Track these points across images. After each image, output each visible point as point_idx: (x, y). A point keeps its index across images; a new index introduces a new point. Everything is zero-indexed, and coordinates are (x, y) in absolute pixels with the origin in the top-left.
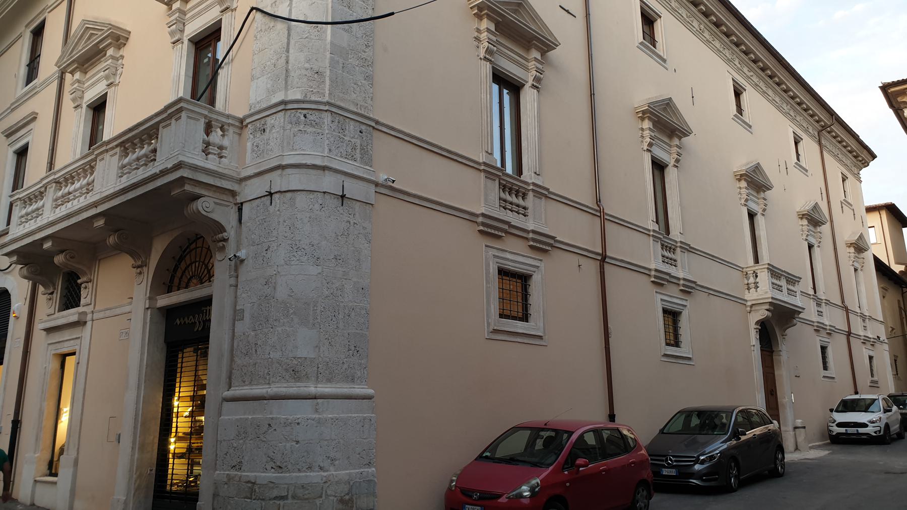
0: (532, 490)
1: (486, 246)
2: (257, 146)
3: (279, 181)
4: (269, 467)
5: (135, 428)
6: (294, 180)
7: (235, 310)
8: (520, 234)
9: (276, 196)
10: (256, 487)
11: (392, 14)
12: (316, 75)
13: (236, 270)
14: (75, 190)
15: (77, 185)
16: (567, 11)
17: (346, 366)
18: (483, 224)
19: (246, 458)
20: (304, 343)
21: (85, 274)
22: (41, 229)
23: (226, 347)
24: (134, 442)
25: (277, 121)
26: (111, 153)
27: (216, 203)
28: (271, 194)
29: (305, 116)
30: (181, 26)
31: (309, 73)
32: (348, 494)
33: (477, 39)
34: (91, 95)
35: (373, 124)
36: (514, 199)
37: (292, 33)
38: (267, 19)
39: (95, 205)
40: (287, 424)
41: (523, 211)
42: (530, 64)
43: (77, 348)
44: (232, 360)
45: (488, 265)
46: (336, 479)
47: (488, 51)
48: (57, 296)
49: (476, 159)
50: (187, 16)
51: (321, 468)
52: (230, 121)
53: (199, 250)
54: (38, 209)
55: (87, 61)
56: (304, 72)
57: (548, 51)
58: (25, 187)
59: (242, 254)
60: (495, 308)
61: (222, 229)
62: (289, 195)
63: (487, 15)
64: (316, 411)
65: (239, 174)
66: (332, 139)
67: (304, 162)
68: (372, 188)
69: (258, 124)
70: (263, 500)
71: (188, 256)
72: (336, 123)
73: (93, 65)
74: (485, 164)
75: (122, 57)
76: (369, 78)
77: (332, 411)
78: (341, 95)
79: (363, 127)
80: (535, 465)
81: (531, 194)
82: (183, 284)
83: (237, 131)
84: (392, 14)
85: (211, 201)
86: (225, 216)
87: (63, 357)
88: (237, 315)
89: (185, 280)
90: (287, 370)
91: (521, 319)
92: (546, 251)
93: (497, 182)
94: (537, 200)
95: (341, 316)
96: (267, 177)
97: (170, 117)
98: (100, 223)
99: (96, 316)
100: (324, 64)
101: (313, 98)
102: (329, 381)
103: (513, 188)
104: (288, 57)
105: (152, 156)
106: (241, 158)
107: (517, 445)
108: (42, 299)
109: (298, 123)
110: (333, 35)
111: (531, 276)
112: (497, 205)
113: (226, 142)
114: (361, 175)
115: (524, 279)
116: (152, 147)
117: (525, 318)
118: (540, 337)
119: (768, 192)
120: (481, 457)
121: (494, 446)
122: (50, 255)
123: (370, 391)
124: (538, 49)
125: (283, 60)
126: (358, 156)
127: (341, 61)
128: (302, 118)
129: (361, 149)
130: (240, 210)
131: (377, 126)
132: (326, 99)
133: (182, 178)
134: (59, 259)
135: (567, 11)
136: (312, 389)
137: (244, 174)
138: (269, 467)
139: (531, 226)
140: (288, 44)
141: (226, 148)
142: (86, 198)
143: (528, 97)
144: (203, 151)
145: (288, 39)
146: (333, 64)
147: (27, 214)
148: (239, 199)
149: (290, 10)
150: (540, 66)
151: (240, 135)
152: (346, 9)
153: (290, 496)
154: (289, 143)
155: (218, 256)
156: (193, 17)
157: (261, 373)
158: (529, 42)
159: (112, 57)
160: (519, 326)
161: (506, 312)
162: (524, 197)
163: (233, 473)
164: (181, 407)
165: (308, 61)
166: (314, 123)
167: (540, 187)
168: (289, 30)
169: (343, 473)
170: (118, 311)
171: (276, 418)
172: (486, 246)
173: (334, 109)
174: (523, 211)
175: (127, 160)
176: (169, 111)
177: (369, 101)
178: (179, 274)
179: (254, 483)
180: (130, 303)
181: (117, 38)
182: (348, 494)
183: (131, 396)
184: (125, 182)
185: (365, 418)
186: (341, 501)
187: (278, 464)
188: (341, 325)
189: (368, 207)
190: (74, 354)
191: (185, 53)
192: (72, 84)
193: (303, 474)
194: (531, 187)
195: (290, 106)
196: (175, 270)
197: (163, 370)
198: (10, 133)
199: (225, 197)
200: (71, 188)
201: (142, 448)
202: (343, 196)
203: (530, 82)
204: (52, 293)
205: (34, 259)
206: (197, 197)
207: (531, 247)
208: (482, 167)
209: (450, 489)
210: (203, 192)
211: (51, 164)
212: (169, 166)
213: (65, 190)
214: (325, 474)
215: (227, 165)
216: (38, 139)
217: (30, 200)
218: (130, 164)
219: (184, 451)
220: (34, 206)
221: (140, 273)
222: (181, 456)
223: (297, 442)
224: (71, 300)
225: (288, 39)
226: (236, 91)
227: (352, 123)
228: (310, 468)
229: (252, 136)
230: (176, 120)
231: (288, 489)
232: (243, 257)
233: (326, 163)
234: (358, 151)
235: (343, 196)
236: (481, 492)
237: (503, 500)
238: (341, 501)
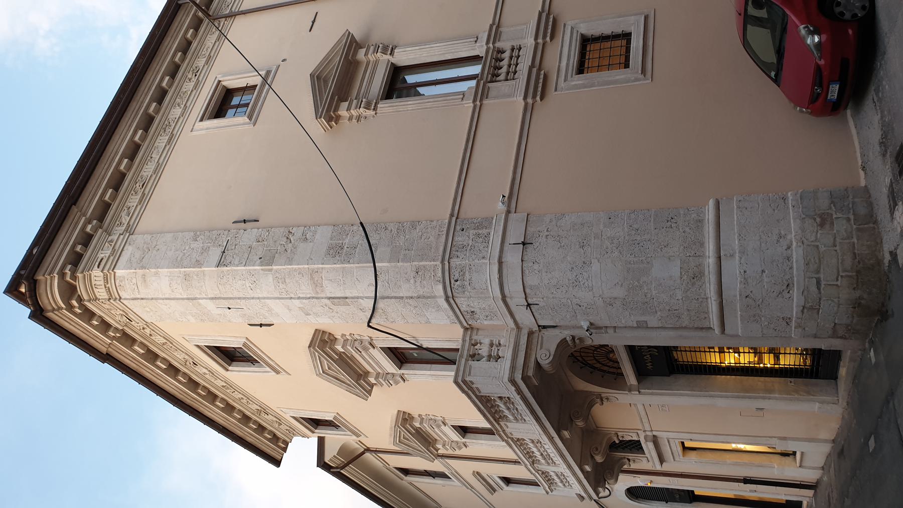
0: (812, 33)
1: (556, 90)
3: (517, 300)
4: (788, 295)
5: (750, 398)
6: (514, 287)
7: (638, 327)
8: (540, 51)
9: (530, 301)
10: (807, 305)
11: (361, 223)
13: (600, 328)
14: (539, 451)
15: (534, 450)
16: (313, 22)
17: (687, 229)
18: (534, 97)
19: (779, 314)
20: (667, 271)
21: (610, 438)
22: (574, 474)
23: (672, 333)
24: (764, 398)
25: (463, 303)
26: (505, 428)
27: (541, 348)
28: (529, 305)
29: (457, 281)
30: (389, 376)
31: (419, 280)
32: (815, 219)
33: (359, 118)
34: (455, 436)
35: (454, 219)
36: (505, 63)
37: (386, 295)
38: (376, 315)
39: (551, 439)
40: (745, 282)
41: (516, 50)
42: (371, 59)
43: (677, 441)
44: (685, 328)
45: (576, 87)
46: (800, 232)
47: (367, 107)
48: (631, 456)
49: (471, 110)
50: (379, 371)
51: (789, 247)
52: (468, 339)
53: (583, 354)
54: (557, 475)
55: (426, 441)
56: (418, 284)
57: (356, 41)
59: (585, 325)
60: (619, 74)
61: (564, 341)
62: (528, 291)
63: (334, 112)
64: (732, 256)
65: (512, 329)
67: (497, 280)
68: (512, 216)
69: (467, 317)
70: (820, 299)
71: (586, 359)
72: (459, 254)
73: (429, 435)
74: (474, 101)
75: (420, 416)
76: (414, 225)
77: (731, 241)
78: (433, 250)
79: (458, 228)
80: (784, 30)
81: (498, 45)
82: (616, 365)
83: (475, 332)
84: (361, 223)
85: (539, 352)
86: (551, 340)
87: (685, 448)
88: (642, 326)
89: (611, 364)
90: (693, 284)
91: (629, 42)
92: (555, 21)
93: (490, 85)
94: (504, 37)
95: (639, 238)
96: (513, 308)
97: (471, 389)
98: (566, 434)
99: (647, 428)
100: (408, 267)
101: (440, 274)
102: (702, 245)
103: (495, 66)
104: (407, 298)
105: (508, 401)
106: (498, 328)
107: (761, 37)
108: (634, 466)
109: (463, 286)
110: (382, 261)
111: (582, 35)
112: (513, 82)
113: (486, 341)
114: (502, 224)
115: (586, 41)
116: (498, 400)
117: (627, 36)
118: (646, 18)
120: (776, 81)
122: (596, 466)
123: (711, 203)
124: (355, 53)
125: (411, 301)
126: (485, 231)
127: (403, 252)
128: (458, 283)
130: (544, 327)
131: (455, 215)
132: (439, 263)
133: (523, 379)
134: (599, 459)
135: (313, 22)
136: (711, 261)
137: (512, 325)
138: (788, 295)
139: (530, 42)
140: (396, 298)
141: (492, 341)
143: (402, 58)
145: (392, 298)
146: (410, 260)
147: (562, 482)
148: (536, 328)
149: (366, 298)
150: (372, 48)
151: (478, 329)
152: (357, 250)
154: (482, 293)
155: (588, 342)
156: (380, 367)
158: (351, 63)
159: (421, 423)
160: (636, 43)
161: (623, 60)
162: (501, 51)
163: (793, 324)
164: (730, 359)
165: (408, 280)
167: (489, 36)
168: (383, 298)
169: (794, 225)
170: (643, 413)
171: (740, 291)
172: (556, 90)
173: (446, 258)
174: (516, 50)
175: (511, 417)
176: (466, 389)
177: (434, 223)
178: (606, 368)
179: (804, 307)
180: (635, 405)
181: (405, 420)
182: (815, 219)
183: (721, 402)
184: (529, 418)
185: (738, 207)
186: (822, 225)
187: (785, 287)
188: (647, 237)
189: (530, 219)
190: (683, 443)
191: (411, 372)
192: (447, 450)
193: (795, 264)
194: (491, 45)
195: (450, 294)
196: (600, 370)
197: (695, 377)
198: (492, 490)
199: (535, 341)
200: (537, 454)
201: (770, 391)
202: (524, 244)
203: (388, 57)
204: (629, 460)
205: (599, 477)
206: (538, 365)
207: (552, 38)
208: (478, 103)
209: (811, 113)
210: (533, 360)
211: (515, 462)
212: (513, 388)
213: (540, 458)
214: (794, 244)
215: (507, 340)
216: (495, 471)
217: (549, 480)
218: (513, 415)
219: (772, 355)
220: (555, 478)
221: (607, 399)
222: (777, 358)
223: (763, 271)
224: (636, 447)
225: (392, 298)
226: (441, 332)
227: (456, 239)
228: (788, 259)
230: (473, 383)
231: (810, 278)
232: (588, 324)
233: (496, 261)
234: (480, 232)
235: (524, 244)
236: (814, 85)
237: (822, 62)
238: (822, 225)
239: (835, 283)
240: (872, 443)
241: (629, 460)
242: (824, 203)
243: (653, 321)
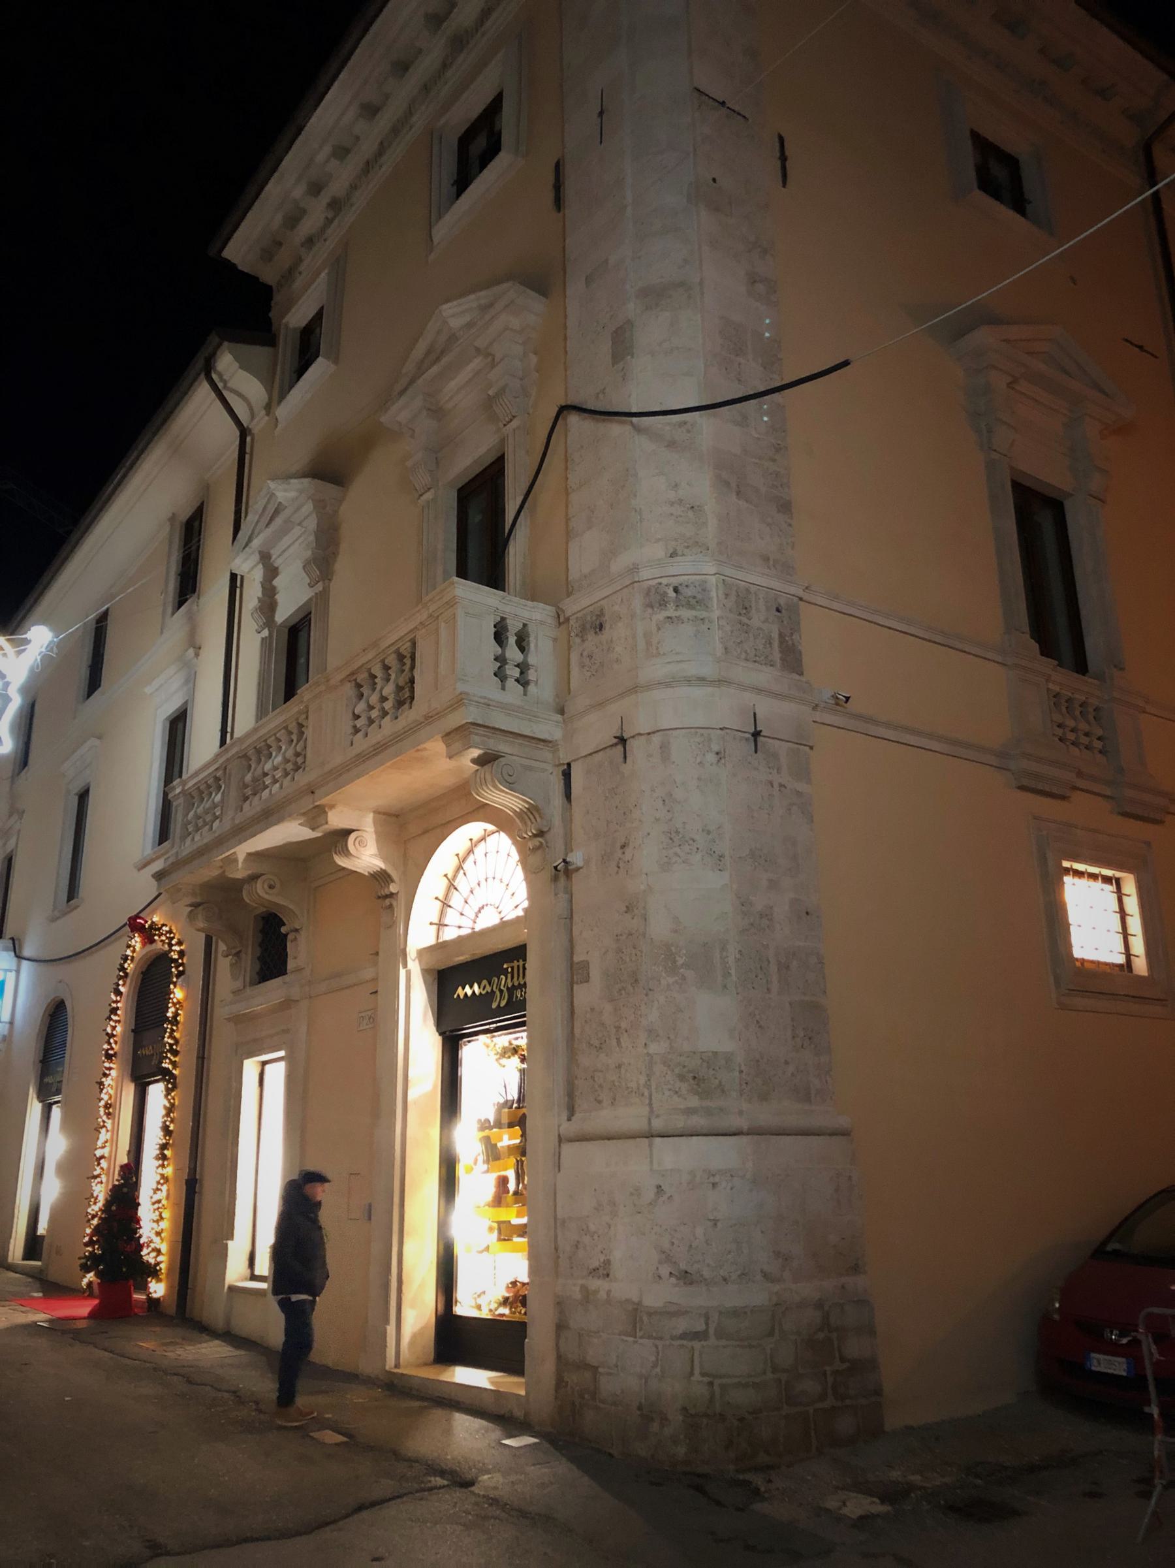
2: (590, 657)
12: (690, 514)
17: (791, 1069)
58: (184, 776)
66: (728, 628)
88: (576, 973)
90: (682, 1078)
119: (327, 1185)
120: (1099, 1252)
121: (1125, 1226)
126: (777, 656)
129: (781, 643)
142: (193, 839)
144: (495, 674)
153: (711, 1331)
157: (633, 1085)
163: (595, 1284)
166: (693, 601)
187: (683, 1266)
229: (578, 640)
239: (697, 1371)
240: (331, 1437)
241: (238, 954)
242: (855, 1348)
243: (585, 996)
